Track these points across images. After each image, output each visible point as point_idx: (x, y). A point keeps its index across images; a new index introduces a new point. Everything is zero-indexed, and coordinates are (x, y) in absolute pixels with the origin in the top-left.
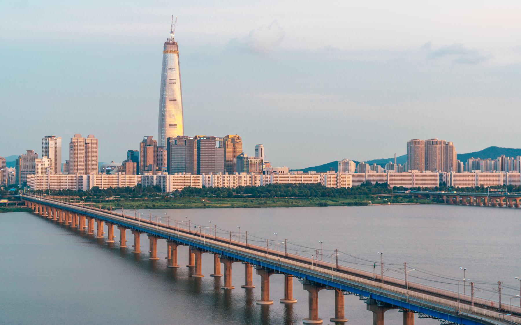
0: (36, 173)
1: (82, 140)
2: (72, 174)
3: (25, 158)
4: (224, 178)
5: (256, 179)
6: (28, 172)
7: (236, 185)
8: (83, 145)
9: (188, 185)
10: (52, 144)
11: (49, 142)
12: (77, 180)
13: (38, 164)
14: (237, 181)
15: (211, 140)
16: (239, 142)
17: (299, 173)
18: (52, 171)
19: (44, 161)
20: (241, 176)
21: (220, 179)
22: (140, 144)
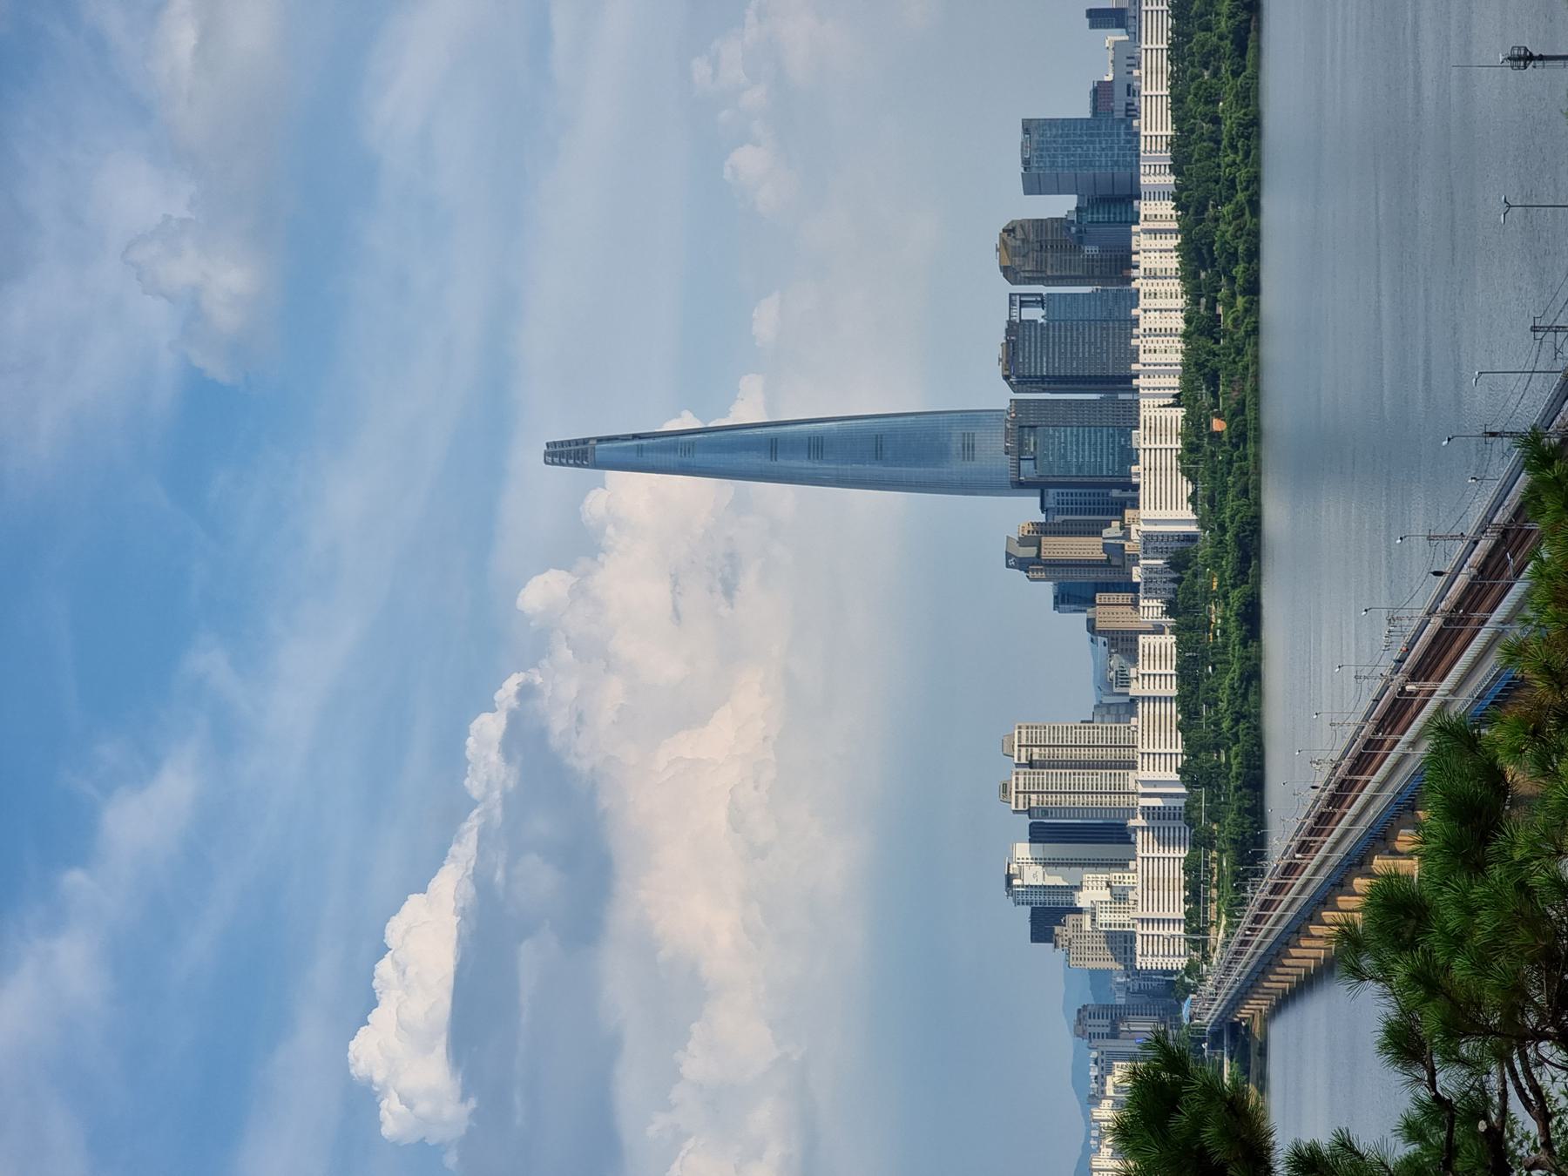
0: (1131, 929)
1: (1021, 778)
2: (1133, 812)
3: (1079, 956)
4: (1150, 329)
5: (1156, 216)
6: (1125, 947)
7: (1176, 286)
8: (1038, 731)
9: (1182, 944)
10: (1035, 876)
11: (1025, 884)
12: (1156, 823)
13: (1101, 924)
14: (1160, 284)
15: (1017, 336)
16: (1023, 230)
17: (1135, 10)
18: (1124, 877)
19: (1092, 902)
20: (1145, 269)
21: (1155, 344)
22: (1032, 580)
